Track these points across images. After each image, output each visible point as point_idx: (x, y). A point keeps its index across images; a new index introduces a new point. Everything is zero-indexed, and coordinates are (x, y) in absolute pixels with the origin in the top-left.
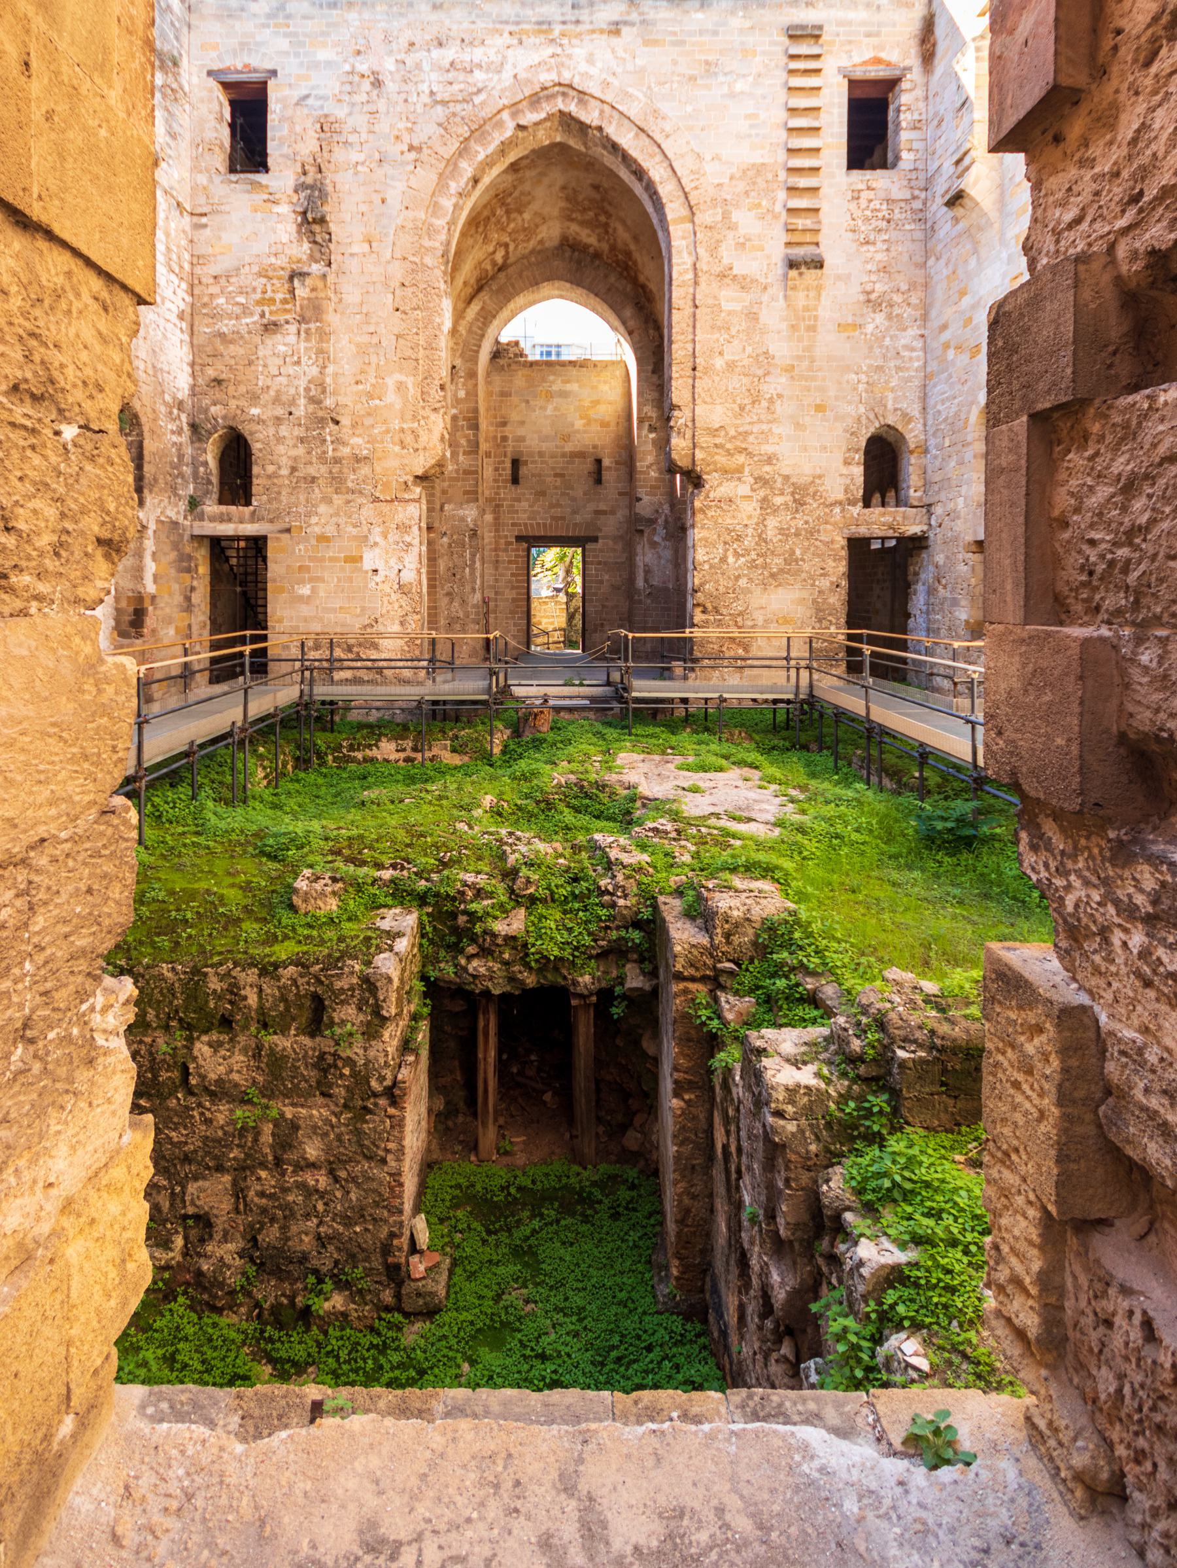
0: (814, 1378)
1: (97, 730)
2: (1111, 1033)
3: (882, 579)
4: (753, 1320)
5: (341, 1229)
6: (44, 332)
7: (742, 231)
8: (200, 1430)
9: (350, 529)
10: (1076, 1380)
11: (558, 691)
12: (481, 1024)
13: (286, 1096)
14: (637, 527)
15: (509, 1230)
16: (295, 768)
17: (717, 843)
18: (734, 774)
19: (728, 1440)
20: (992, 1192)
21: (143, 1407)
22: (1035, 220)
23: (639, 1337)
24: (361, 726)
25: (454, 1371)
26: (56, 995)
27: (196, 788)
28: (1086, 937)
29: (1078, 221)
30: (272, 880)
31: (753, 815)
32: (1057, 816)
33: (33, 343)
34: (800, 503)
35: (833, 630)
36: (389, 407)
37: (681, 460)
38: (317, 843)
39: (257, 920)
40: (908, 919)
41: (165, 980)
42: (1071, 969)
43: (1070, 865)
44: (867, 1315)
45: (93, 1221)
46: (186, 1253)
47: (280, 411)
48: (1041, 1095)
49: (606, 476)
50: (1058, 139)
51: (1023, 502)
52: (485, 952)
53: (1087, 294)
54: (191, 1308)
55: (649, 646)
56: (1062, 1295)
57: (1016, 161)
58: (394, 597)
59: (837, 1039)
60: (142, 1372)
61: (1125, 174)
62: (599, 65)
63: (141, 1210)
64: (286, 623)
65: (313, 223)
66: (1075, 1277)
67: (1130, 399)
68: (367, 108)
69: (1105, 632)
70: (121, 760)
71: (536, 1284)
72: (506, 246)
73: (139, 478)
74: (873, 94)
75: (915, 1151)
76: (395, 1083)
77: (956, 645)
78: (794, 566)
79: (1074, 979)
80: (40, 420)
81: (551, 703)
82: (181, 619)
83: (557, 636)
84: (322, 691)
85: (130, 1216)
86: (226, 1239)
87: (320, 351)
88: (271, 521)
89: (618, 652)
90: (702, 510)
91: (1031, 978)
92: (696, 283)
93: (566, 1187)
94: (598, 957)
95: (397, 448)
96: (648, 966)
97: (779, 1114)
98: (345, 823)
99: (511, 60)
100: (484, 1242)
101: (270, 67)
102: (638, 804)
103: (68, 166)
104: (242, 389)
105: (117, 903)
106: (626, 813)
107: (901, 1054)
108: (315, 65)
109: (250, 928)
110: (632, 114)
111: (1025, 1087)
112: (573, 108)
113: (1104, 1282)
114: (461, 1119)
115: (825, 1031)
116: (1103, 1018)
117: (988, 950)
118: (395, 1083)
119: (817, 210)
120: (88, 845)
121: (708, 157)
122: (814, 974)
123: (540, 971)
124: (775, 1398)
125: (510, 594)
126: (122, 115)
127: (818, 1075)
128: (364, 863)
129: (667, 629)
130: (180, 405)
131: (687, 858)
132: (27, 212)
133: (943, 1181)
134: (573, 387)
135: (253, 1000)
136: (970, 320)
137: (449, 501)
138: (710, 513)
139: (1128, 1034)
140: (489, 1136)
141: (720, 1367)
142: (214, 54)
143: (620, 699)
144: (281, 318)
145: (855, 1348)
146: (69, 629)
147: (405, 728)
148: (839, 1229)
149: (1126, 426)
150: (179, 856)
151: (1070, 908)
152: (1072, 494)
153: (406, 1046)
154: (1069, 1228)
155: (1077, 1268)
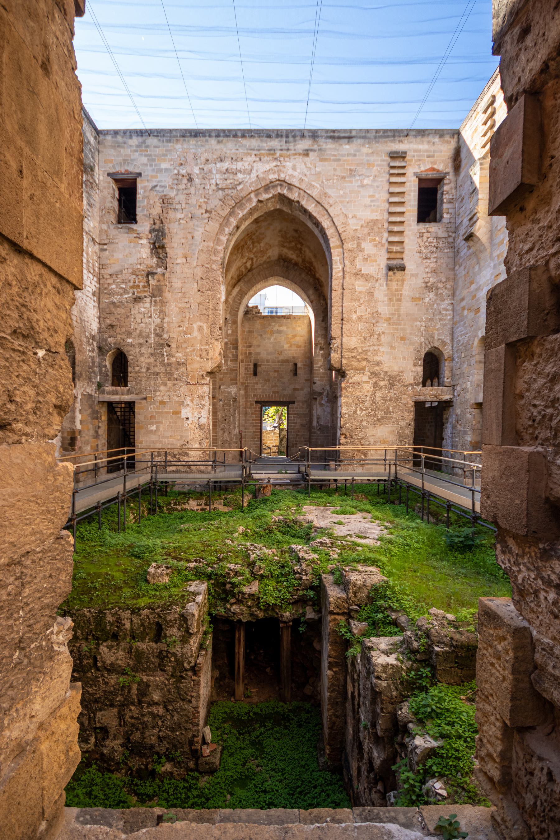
0: (393, 800)
1: (54, 499)
2: (538, 640)
3: (430, 421)
4: (364, 774)
5: (170, 733)
6: (29, 304)
7: (366, 252)
8: (105, 828)
9: (175, 398)
10: (515, 799)
11: (275, 476)
12: (237, 636)
13: (143, 671)
14: (314, 396)
15: (249, 733)
16: (148, 513)
17: (350, 549)
18: (359, 515)
19: (353, 831)
20: (479, 714)
21: (77, 818)
22: (510, 249)
23: (310, 782)
24: (180, 493)
25: (223, 799)
26: (35, 627)
27: (100, 524)
28: (527, 595)
29: (531, 249)
30: (137, 568)
31: (368, 535)
32: (515, 537)
33: (24, 309)
34: (392, 385)
35: (407, 446)
36: (195, 338)
37: (336, 365)
38: (159, 550)
39: (130, 587)
40: (441, 584)
41: (86, 616)
42: (520, 610)
43: (520, 560)
44: (419, 771)
45: (53, 733)
46: (96, 745)
47: (142, 341)
48: (504, 670)
49: (299, 371)
50: (522, 209)
51: (502, 386)
52: (239, 602)
53: (535, 285)
54: (99, 770)
55: (318, 455)
56: (511, 762)
57: (501, 221)
58: (196, 431)
59: (406, 642)
60: (76, 800)
61: (554, 227)
62: (298, 171)
63: (75, 727)
64: (144, 444)
65: (158, 248)
66: (517, 753)
67: (555, 336)
68: (185, 192)
69: (540, 449)
70: (66, 513)
71: (262, 758)
72: (252, 259)
73: (74, 373)
74: (430, 185)
75: (442, 694)
76: (196, 664)
77: (466, 453)
78: (389, 415)
79: (521, 614)
80: (27, 347)
81: (272, 482)
82: (93, 442)
83: (275, 449)
84: (161, 477)
85: (70, 730)
86: (115, 738)
87: (161, 311)
88: (137, 394)
89: (304, 457)
90: (345, 388)
91: (501, 614)
92: (344, 278)
93: (277, 712)
94: (293, 604)
95: (198, 359)
96: (316, 608)
97: (379, 678)
98: (172, 541)
99: (255, 168)
100: (238, 738)
101: (138, 171)
102: (313, 530)
103: (41, 222)
104: (123, 330)
105: (64, 582)
106: (307, 534)
107: (437, 649)
108: (160, 171)
109: (127, 591)
110: (314, 195)
111: (497, 665)
112: (285, 192)
113: (530, 755)
114: (227, 681)
115: (401, 638)
116: (534, 633)
117: (480, 600)
118: (196, 664)
119: (403, 242)
120: (50, 554)
121: (350, 216)
122: (396, 611)
123: (265, 611)
124: (375, 811)
125: (252, 429)
126: (67, 196)
127: (397, 659)
128: (181, 560)
129: (328, 446)
130: (93, 338)
131: (336, 556)
132: (21, 244)
133: (455, 708)
134: (284, 328)
135: (128, 625)
136: (475, 295)
137: (223, 384)
138: (349, 390)
139: (546, 640)
140: (240, 689)
141: (348, 795)
142: (111, 165)
143: (305, 480)
144: (143, 295)
145: (413, 786)
146: (41, 450)
147: (201, 494)
148: (406, 732)
149: (552, 350)
150: (93, 556)
151: (520, 581)
152: (525, 382)
153: (201, 647)
154: (515, 731)
155: (518, 749)
